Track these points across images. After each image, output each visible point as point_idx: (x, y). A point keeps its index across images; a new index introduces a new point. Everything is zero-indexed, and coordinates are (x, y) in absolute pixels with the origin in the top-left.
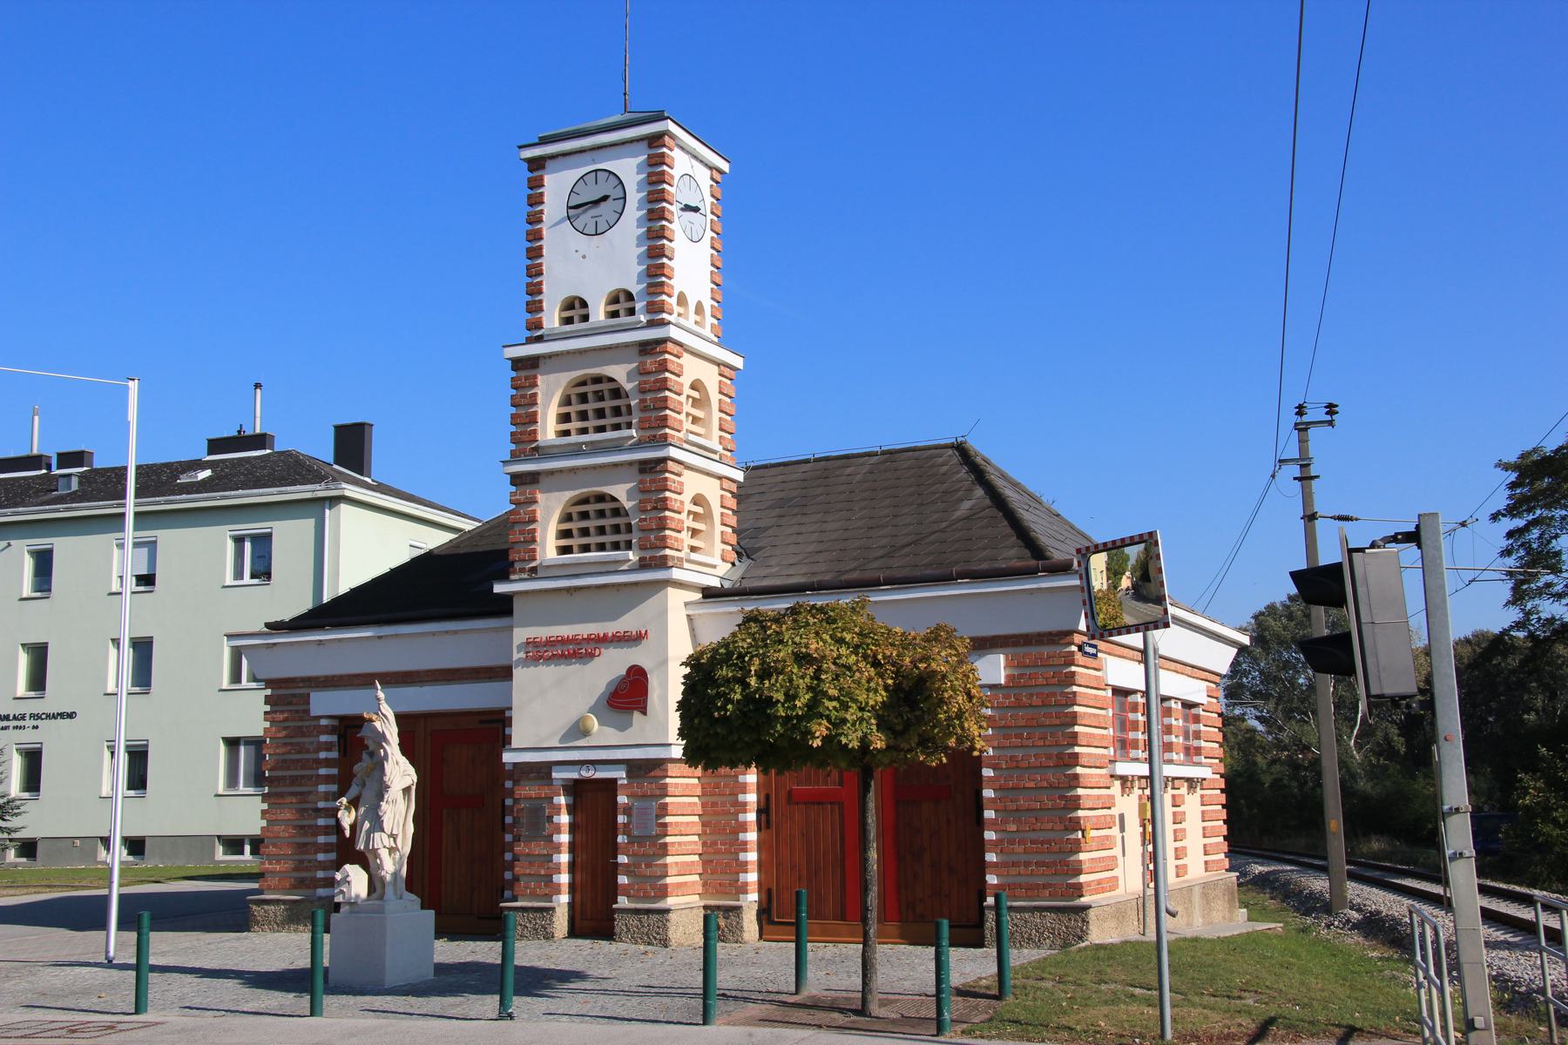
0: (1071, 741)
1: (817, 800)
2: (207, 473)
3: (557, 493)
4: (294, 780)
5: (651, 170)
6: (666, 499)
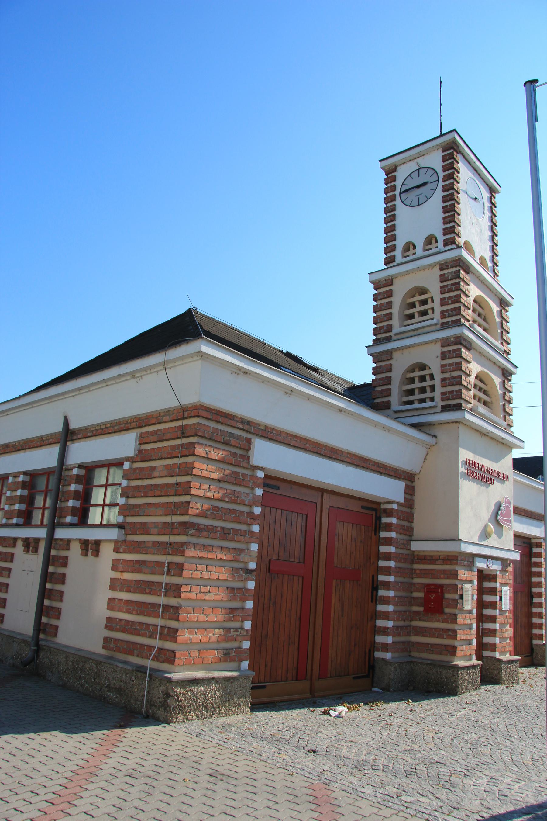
4: (225, 534)
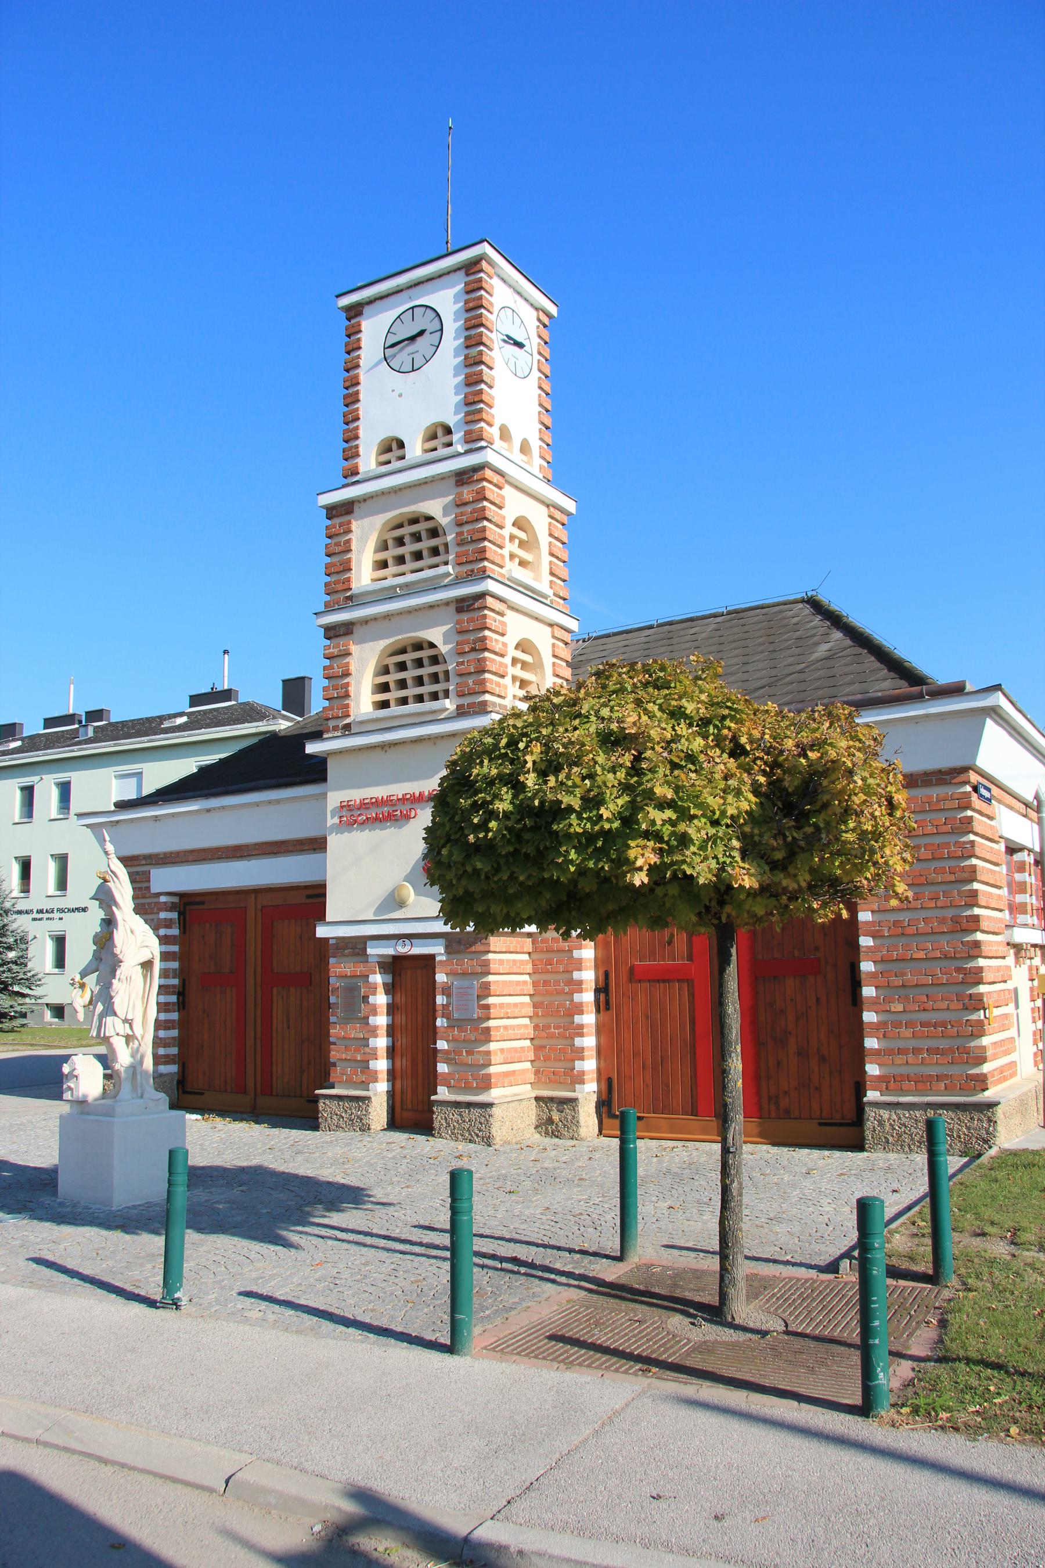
0: (969, 900)
1: (663, 977)
2: (185, 719)
3: (371, 643)
5: (468, 297)
6: (485, 638)
